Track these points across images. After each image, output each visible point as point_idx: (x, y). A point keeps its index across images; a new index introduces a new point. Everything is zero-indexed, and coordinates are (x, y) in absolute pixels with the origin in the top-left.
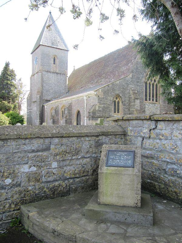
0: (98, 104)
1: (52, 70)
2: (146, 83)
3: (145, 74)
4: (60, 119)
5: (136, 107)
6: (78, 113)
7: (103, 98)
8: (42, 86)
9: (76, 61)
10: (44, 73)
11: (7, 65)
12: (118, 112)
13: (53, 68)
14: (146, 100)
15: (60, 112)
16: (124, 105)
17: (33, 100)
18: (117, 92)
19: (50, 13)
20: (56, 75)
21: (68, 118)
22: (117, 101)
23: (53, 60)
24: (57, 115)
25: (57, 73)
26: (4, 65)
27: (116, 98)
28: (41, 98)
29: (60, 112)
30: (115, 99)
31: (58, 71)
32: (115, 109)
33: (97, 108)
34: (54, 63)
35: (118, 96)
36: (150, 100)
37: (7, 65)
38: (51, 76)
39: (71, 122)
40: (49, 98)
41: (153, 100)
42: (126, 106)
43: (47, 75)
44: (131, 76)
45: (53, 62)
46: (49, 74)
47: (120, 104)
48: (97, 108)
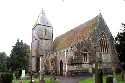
0: (74, 56)
1: (44, 38)
2: (101, 42)
3: (99, 37)
4: (49, 66)
5: (97, 56)
6: (61, 62)
7: (77, 52)
8: (38, 47)
9: (57, 32)
10: (39, 39)
11: (18, 41)
12: (87, 60)
13: (45, 37)
14: (102, 52)
15: (49, 62)
16: (90, 55)
17: (33, 56)
18: (85, 48)
19: (43, 8)
20: (46, 40)
21: (54, 65)
22: (85, 53)
23: (44, 32)
24: (47, 64)
25: (47, 40)
26: (17, 40)
27: (85, 52)
28: (38, 53)
29: (49, 62)
30: (84, 52)
31: (47, 38)
32: (84, 58)
33: (74, 58)
34: (45, 34)
35: (85, 50)
36: (104, 52)
37: (18, 41)
38: (44, 40)
39: (57, 68)
40: (42, 54)
41: (106, 52)
42: (91, 56)
43: (40, 41)
44: (92, 38)
45: (44, 33)
46: (42, 40)
47: (87, 55)
48: (74, 58)
